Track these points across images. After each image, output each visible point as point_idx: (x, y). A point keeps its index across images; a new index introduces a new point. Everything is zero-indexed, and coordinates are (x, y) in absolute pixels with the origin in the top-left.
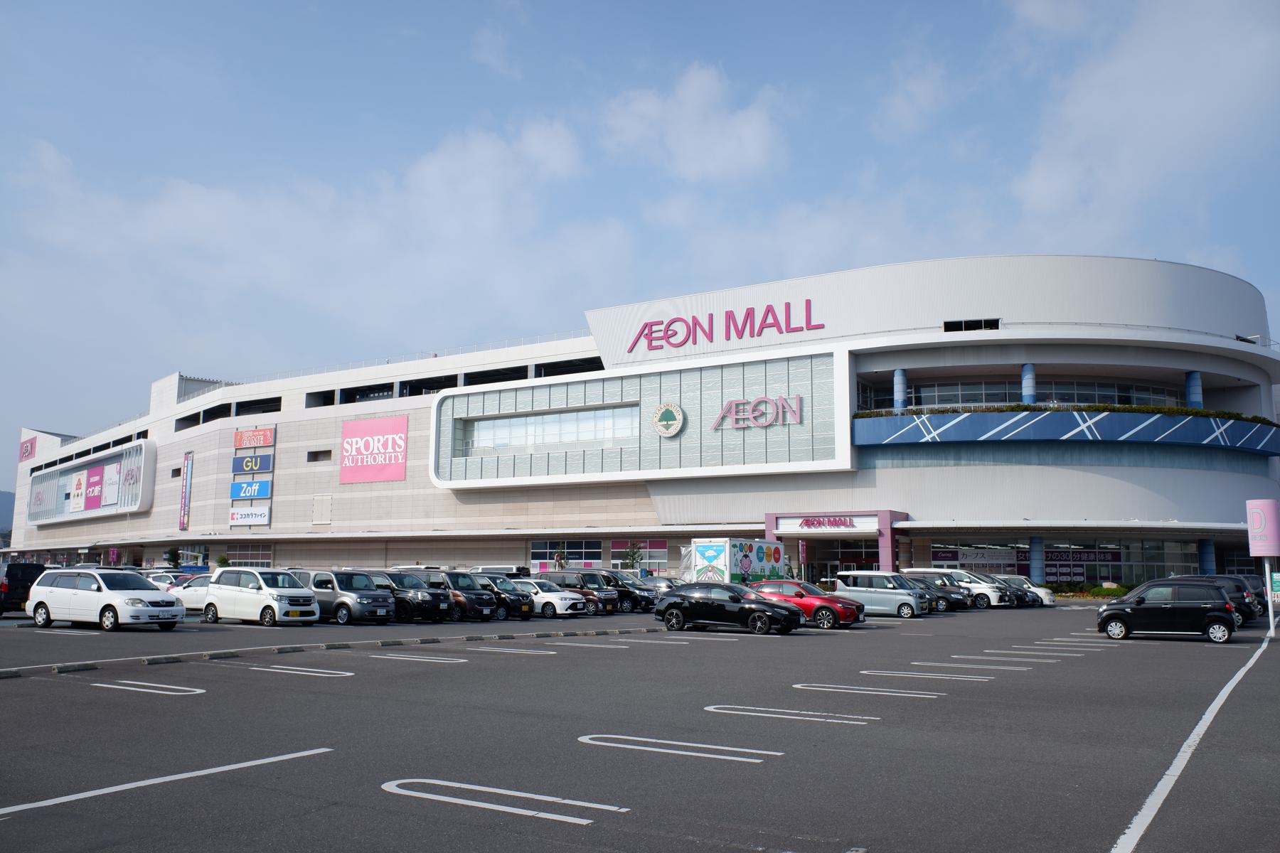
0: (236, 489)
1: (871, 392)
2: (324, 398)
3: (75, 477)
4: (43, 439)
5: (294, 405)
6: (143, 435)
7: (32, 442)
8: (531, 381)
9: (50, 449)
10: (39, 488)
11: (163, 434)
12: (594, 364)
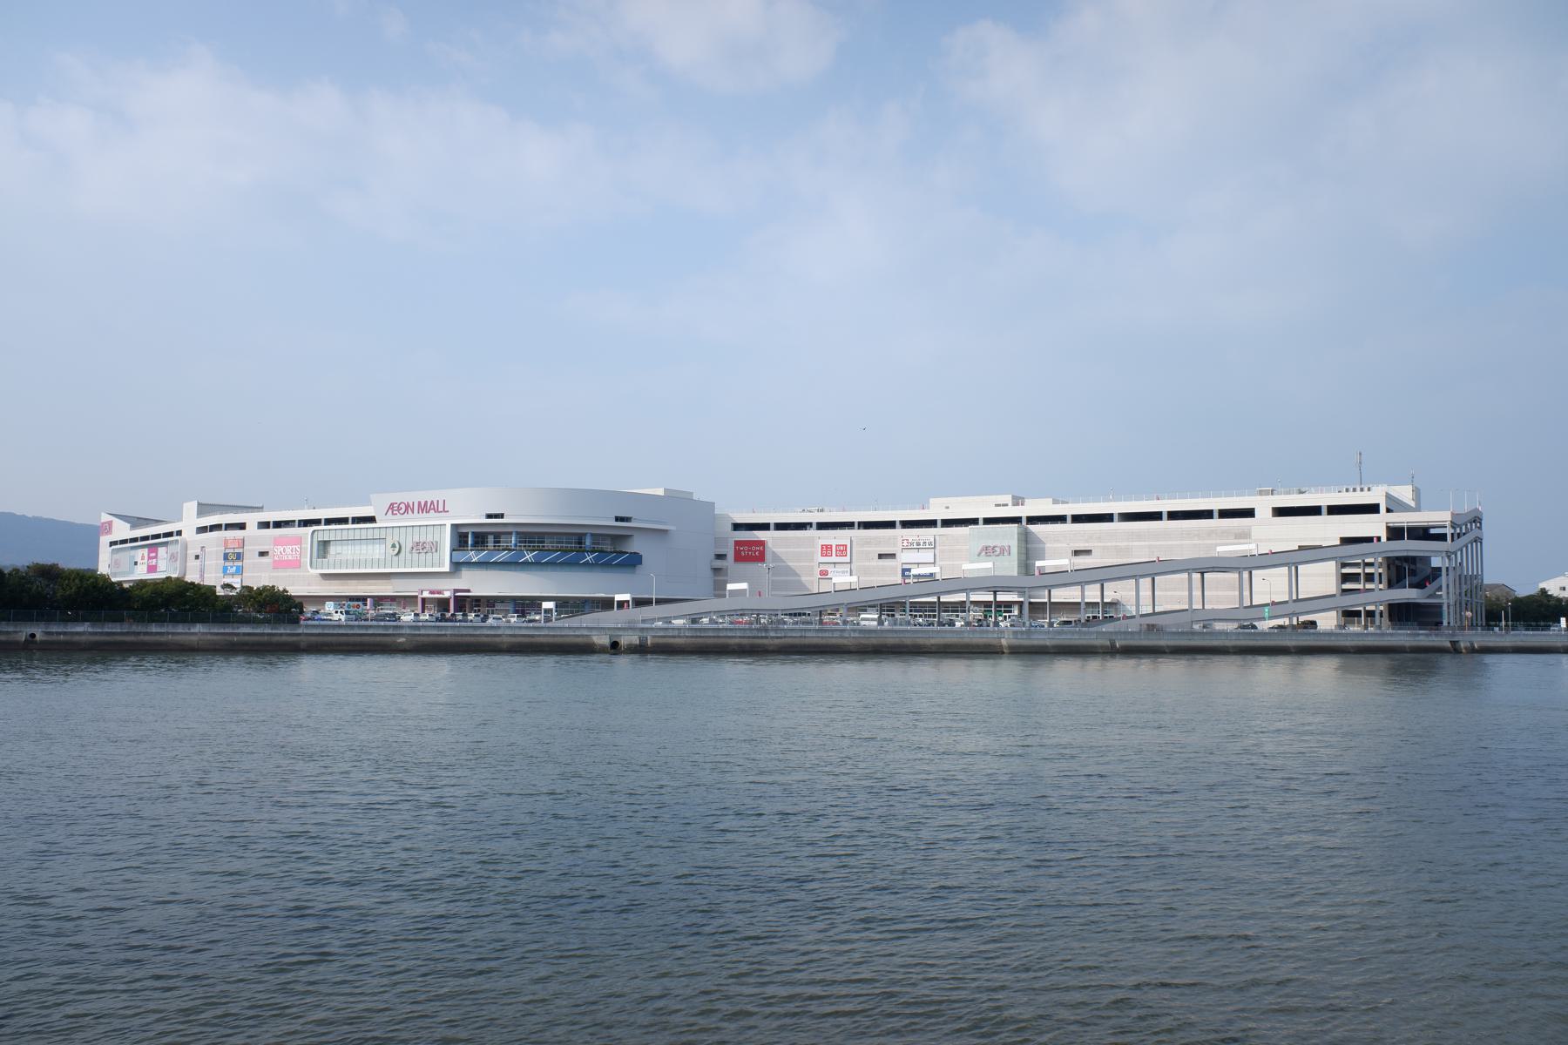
0: (225, 569)
1: (461, 538)
2: (265, 525)
3: (140, 552)
4: (117, 523)
5: (252, 528)
6: (179, 533)
7: (110, 523)
8: (350, 526)
9: (122, 530)
10: (116, 556)
11: (189, 534)
12: (372, 519)
